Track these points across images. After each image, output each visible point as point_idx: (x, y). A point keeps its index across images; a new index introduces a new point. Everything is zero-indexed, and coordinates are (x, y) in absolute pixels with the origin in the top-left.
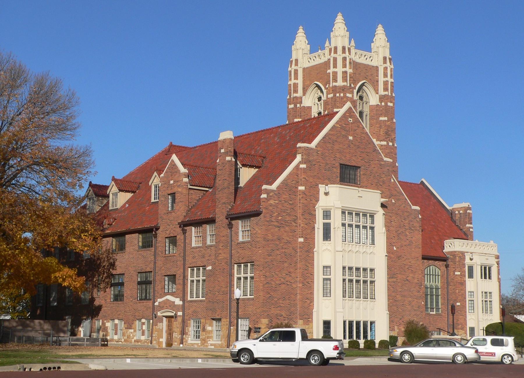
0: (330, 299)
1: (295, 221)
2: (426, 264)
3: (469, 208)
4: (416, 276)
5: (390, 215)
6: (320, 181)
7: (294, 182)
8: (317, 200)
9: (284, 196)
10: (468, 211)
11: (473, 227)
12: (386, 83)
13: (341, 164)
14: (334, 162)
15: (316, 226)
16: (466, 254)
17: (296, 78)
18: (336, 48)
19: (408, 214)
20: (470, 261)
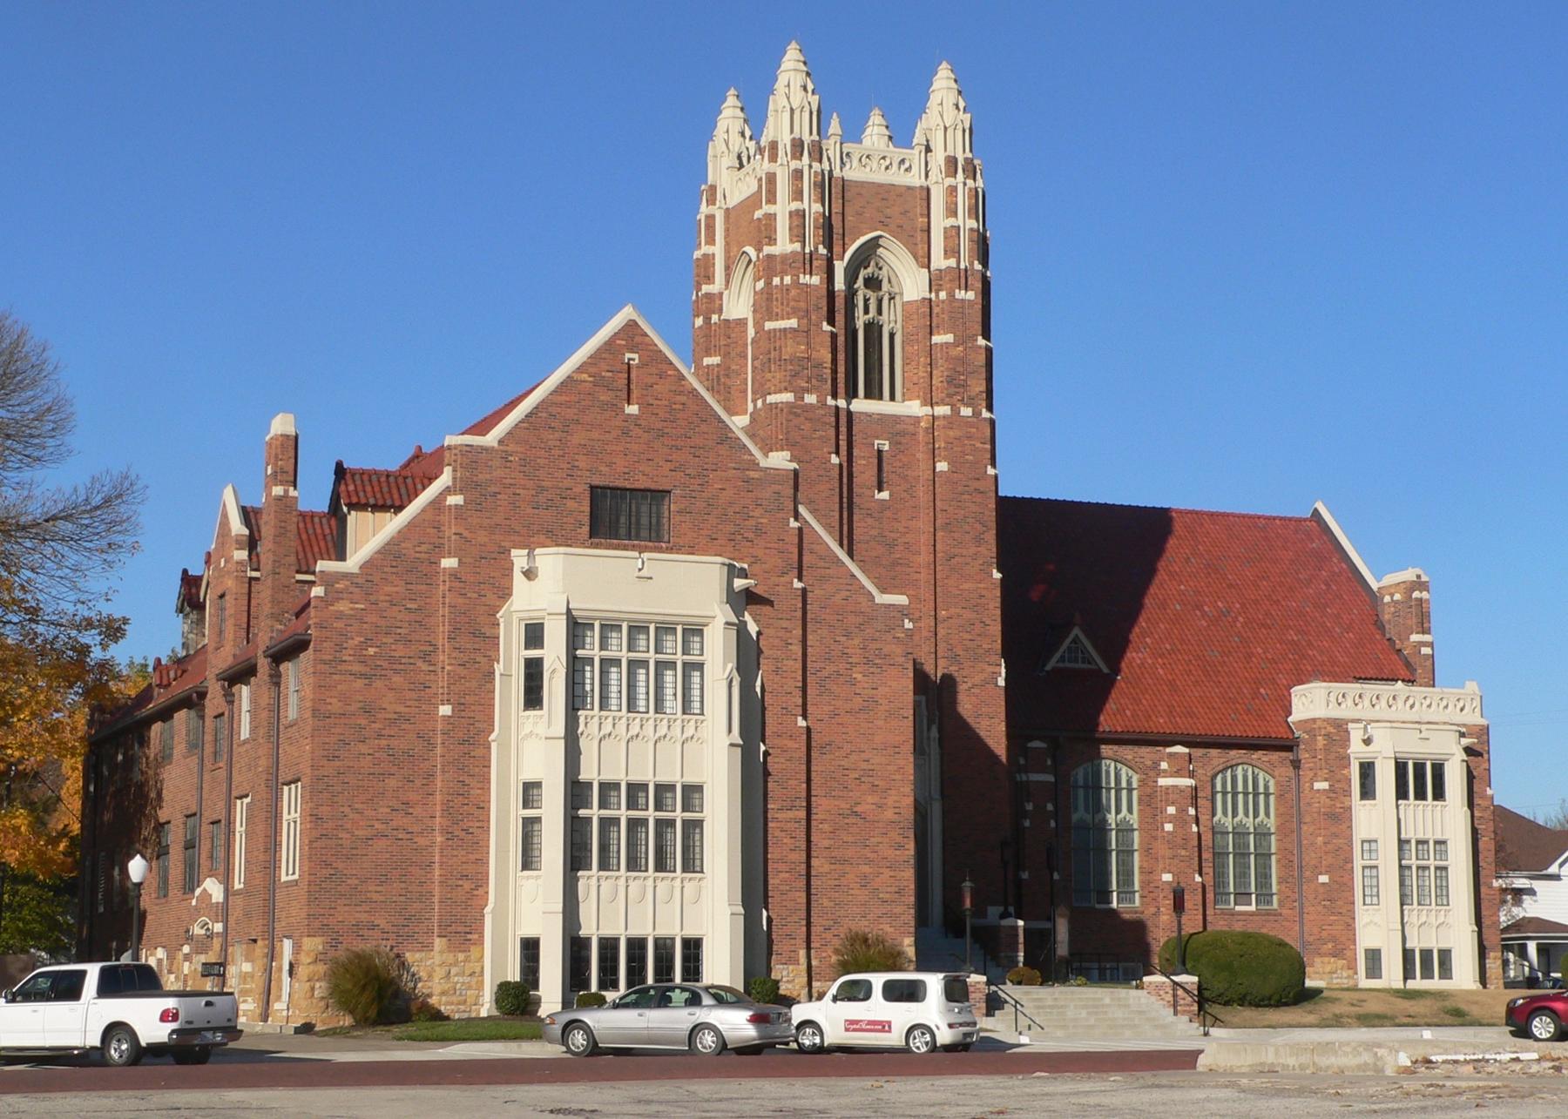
0: (537, 877)
1: (426, 657)
2: (1215, 762)
3: (1419, 585)
4: (890, 801)
5: (785, 624)
6: (517, 538)
7: (424, 548)
8: (505, 593)
9: (388, 589)
10: (1416, 594)
11: (1439, 640)
12: (952, 234)
13: (592, 487)
14: (568, 483)
15: (499, 668)
16: (1351, 726)
17: (711, 240)
18: (774, 146)
19: (860, 620)
20: (1363, 748)
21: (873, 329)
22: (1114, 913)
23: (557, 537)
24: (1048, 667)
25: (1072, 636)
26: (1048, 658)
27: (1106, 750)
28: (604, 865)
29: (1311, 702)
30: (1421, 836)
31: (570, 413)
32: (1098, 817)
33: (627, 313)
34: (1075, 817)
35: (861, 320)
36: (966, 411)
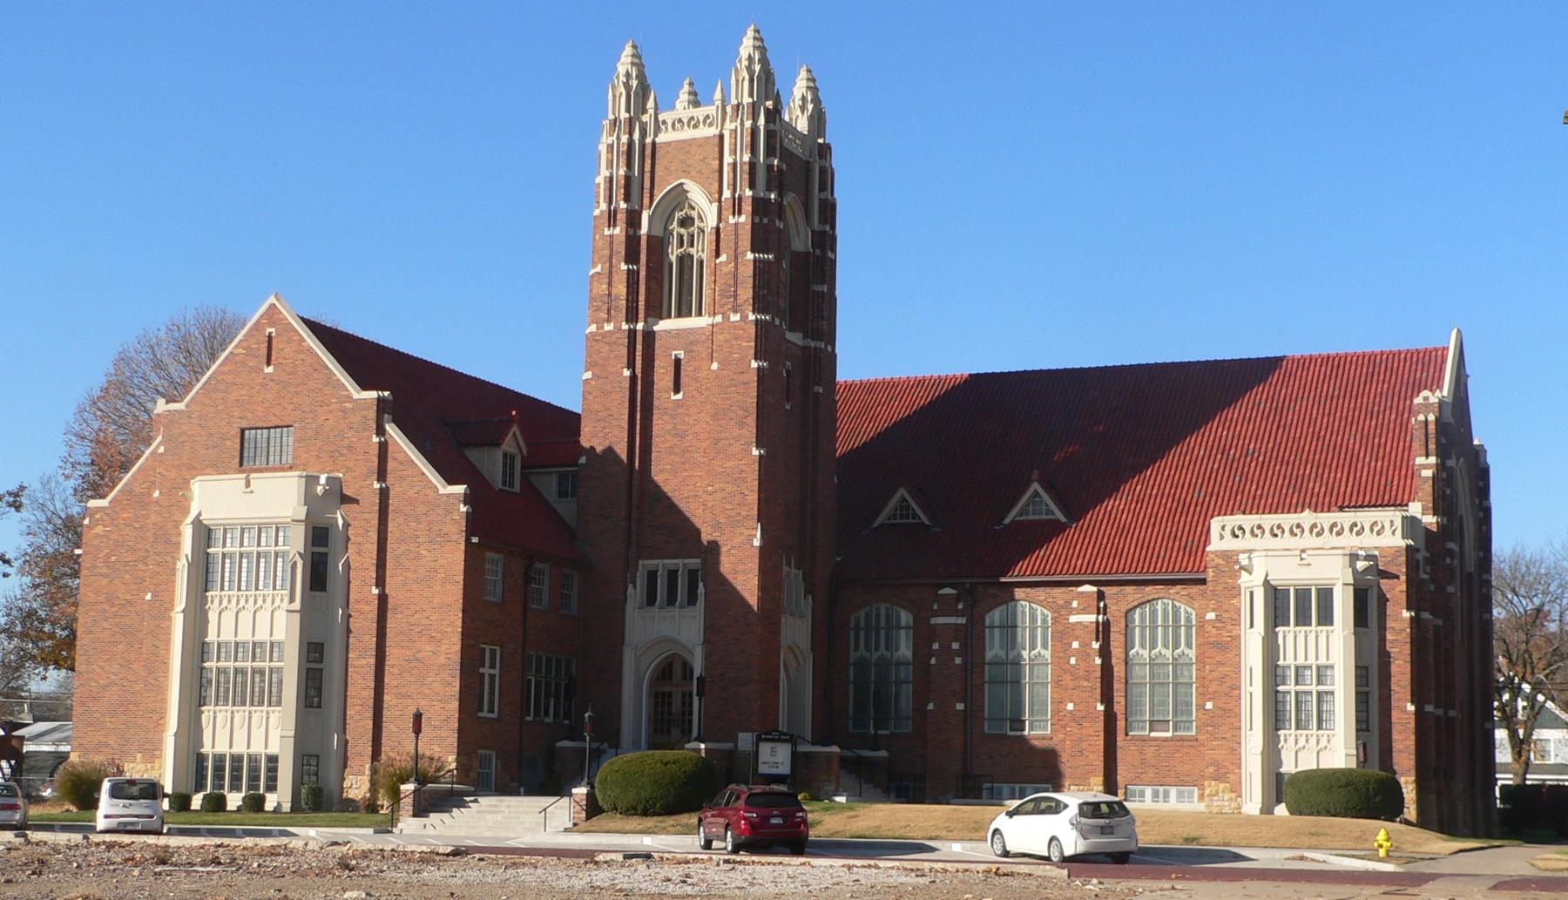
2: (1130, 598)
5: (367, 516)
16: (1241, 556)
21: (685, 260)
22: (1023, 740)
23: (219, 468)
24: (1007, 521)
26: (1007, 512)
27: (1019, 593)
29: (1222, 533)
30: (1301, 661)
31: (229, 378)
32: (1012, 655)
33: (272, 300)
34: (989, 655)
36: (735, 317)
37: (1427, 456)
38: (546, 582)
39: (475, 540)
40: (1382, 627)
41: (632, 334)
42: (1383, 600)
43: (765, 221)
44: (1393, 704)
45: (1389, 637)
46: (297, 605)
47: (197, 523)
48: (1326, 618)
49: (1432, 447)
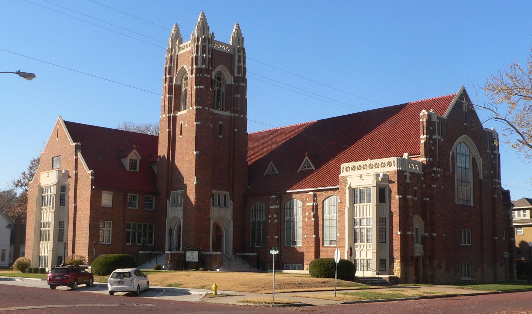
22: (294, 248)
24: (299, 171)
25: (305, 159)
28: (361, 241)
30: (361, 217)
34: (286, 219)
35: (183, 89)
37: (423, 135)
38: (138, 200)
39: (94, 187)
40: (390, 202)
41: (169, 117)
42: (390, 192)
43: (201, 75)
44: (394, 232)
45: (392, 206)
46: (53, 210)
47: (350, 187)
48: (369, 200)
49: (425, 131)
